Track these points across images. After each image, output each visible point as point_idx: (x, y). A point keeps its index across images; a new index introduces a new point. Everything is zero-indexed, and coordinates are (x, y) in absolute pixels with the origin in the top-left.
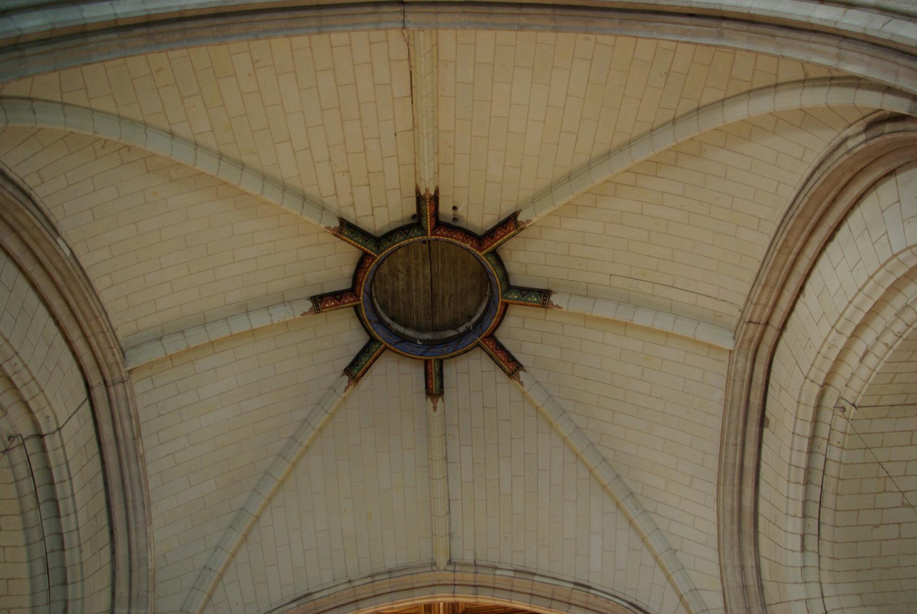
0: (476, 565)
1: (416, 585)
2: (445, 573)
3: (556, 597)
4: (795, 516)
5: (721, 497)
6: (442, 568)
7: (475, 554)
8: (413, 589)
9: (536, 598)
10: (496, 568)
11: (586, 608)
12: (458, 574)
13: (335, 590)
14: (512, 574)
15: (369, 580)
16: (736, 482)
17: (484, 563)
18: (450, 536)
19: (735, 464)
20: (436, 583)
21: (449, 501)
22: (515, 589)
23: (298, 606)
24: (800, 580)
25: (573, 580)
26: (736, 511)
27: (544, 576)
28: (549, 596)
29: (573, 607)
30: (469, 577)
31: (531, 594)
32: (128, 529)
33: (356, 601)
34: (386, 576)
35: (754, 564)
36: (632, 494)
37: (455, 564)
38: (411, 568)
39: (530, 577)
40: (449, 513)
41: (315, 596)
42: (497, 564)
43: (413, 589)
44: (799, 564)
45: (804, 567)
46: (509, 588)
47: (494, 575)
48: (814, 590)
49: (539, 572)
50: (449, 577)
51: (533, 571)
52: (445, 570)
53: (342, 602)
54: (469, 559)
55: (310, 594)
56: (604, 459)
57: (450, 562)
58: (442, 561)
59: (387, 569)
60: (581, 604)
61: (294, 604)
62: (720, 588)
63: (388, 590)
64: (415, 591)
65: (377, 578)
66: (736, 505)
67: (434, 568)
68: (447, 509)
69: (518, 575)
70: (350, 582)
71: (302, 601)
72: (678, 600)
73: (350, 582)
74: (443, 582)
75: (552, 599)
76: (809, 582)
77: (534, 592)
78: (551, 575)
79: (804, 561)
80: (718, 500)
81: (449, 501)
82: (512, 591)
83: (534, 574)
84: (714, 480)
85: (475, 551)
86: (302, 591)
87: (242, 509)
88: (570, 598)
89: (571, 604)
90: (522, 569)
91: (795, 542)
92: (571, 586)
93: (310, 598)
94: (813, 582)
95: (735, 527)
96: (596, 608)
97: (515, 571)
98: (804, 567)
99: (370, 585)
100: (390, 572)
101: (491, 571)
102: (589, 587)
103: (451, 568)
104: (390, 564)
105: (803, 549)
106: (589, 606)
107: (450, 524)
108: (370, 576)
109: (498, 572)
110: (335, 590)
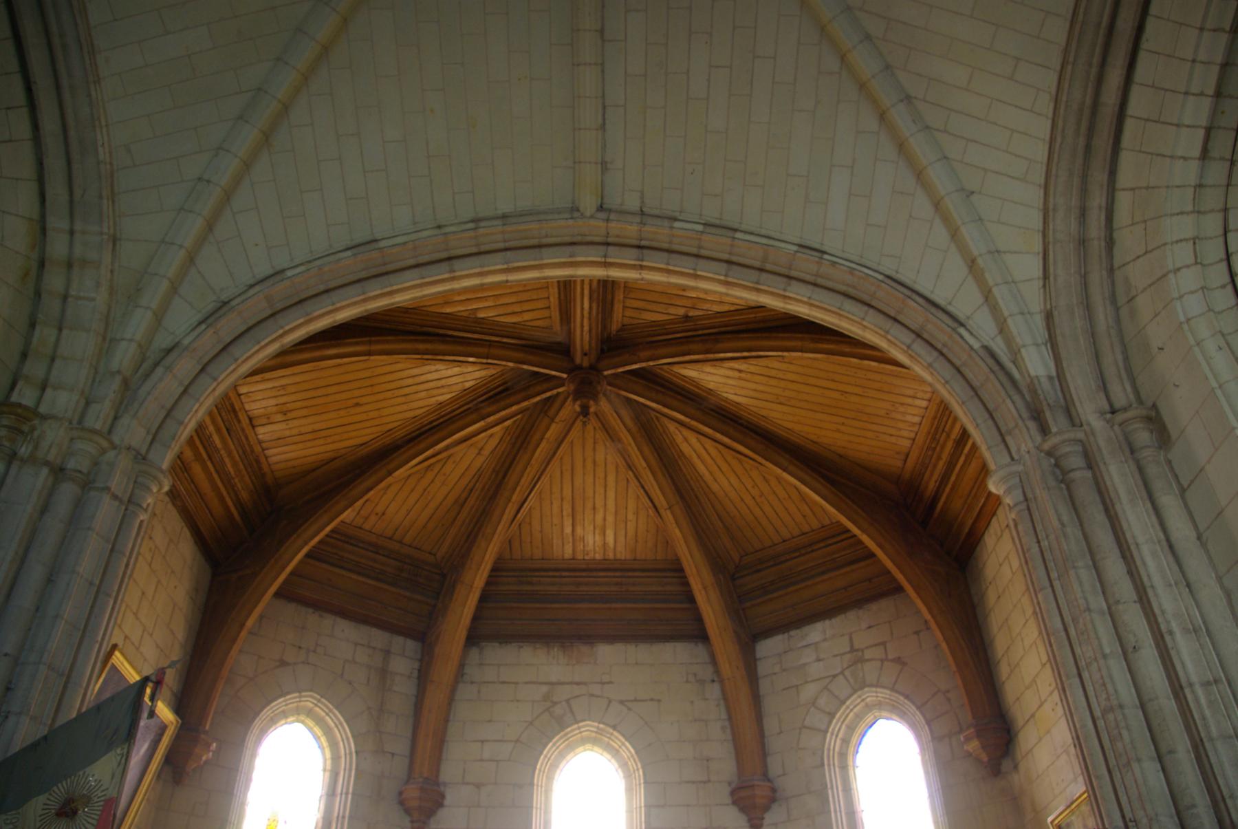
0: (642, 213)
1: (545, 241)
2: (592, 222)
3: (768, 267)
4: (1202, 94)
5: (1074, 46)
6: (588, 214)
7: (642, 198)
8: (540, 246)
9: (735, 267)
10: (676, 219)
11: (815, 285)
12: (612, 225)
13: (413, 237)
14: (700, 228)
15: (471, 225)
16: (1096, 60)
17: (657, 212)
18: (604, 166)
19: (1099, 24)
20: (578, 239)
21: (604, 107)
22: (703, 252)
23: (354, 255)
24: (1190, 208)
25: (797, 241)
26: (1087, 112)
27: (751, 233)
28: (757, 264)
29: (794, 282)
30: (630, 230)
31: (729, 262)
32: (58, 87)
33: (449, 259)
34: (499, 222)
35: (1104, 204)
36: (908, 99)
37: (610, 211)
38: (539, 213)
39: (730, 233)
40: (603, 127)
41: (382, 244)
42: (677, 214)
43: (540, 246)
44: (1192, 179)
45: (1201, 186)
46: (694, 251)
47: (672, 228)
48: (1212, 224)
49: (744, 227)
50: (597, 227)
51: (736, 226)
52: (592, 217)
53: (426, 258)
54: (633, 203)
55: (376, 241)
56: (868, 37)
57: (601, 208)
58: (588, 203)
59: (500, 212)
60: (808, 278)
61: (349, 253)
62: (1038, 247)
63: (501, 245)
64: (544, 250)
65: (482, 224)
66: (1088, 101)
67: (576, 214)
68: (600, 121)
69: (709, 230)
70: (439, 227)
71: (361, 249)
72: (965, 270)
73: (439, 227)
74: (589, 239)
75: (761, 270)
76: (1204, 213)
77: (734, 259)
78: (763, 232)
79: (1201, 177)
80: (1057, 100)
81: (604, 107)
82: (697, 256)
83: (736, 230)
84: (1056, 63)
85: (642, 193)
86: (359, 237)
87: (259, 89)
88: (790, 269)
89: (790, 278)
90: (718, 222)
91: (1191, 143)
92: (795, 248)
93: (374, 245)
94: (1212, 211)
95: (1082, 141)
96: (830, 284)
97: (705, 224)
98: (1201, 186)
99: (472, 234)
100: (504, 217)
101: (666, 223)
102: (824, 253)
103: (602, 215)
104: (504, 207)
105: (1205, 154)
106: (820, 281)
107: (604, 146)
108: (472, 221)
109: (677, 224)
110: (413, 237)
